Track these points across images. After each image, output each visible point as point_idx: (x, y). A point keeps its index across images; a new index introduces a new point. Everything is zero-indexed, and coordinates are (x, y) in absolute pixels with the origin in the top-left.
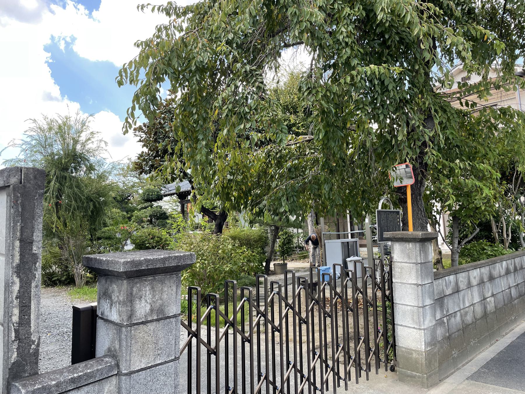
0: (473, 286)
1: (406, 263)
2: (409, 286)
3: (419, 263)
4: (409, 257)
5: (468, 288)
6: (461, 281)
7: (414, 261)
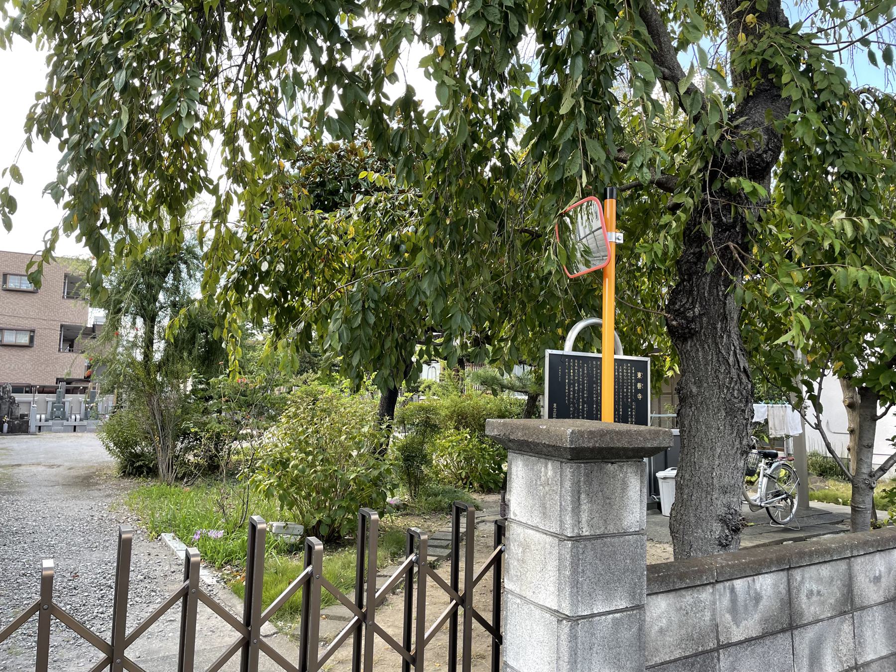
0: (863, 608)
1: (536, 529)
2: (537, 612)
3: (570, 539)
4: (544, 515)
5: (843, 613)
6: (810, 594)
7: (555, 528)
